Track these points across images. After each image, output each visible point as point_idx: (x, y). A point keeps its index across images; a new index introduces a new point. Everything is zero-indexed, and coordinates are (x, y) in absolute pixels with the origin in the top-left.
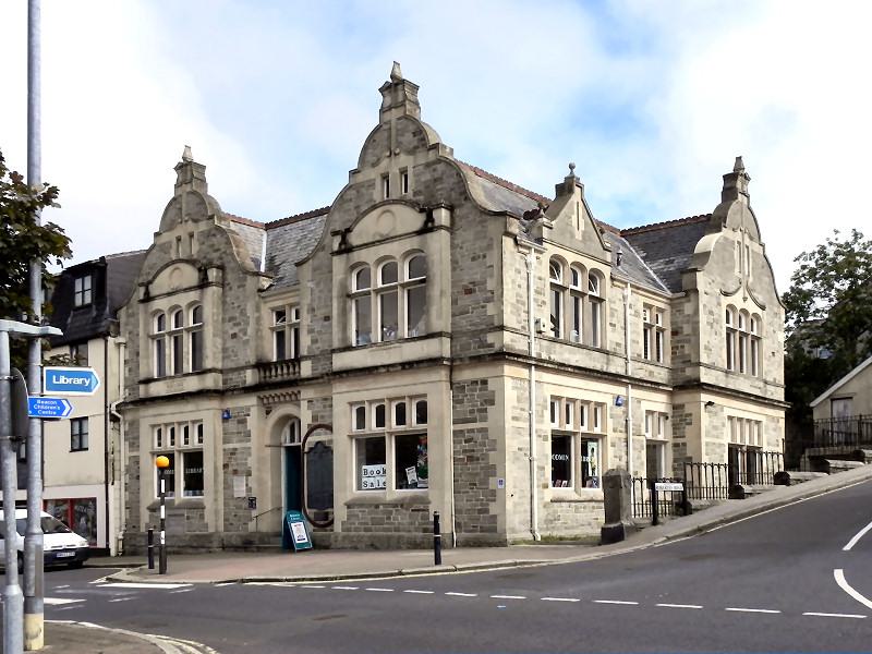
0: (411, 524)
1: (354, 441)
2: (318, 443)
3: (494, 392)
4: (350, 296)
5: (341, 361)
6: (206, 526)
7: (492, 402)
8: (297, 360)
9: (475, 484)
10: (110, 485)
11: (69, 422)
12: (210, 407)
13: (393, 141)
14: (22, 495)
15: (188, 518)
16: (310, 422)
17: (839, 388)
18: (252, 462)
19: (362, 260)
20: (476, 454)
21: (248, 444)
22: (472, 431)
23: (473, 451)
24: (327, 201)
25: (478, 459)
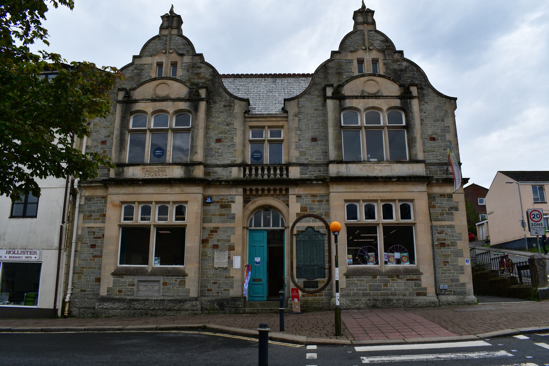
4: (342, 127)
5: (334, 170)
6: (188, 291)
9: (448, 262)
10: (62, 251)
14: (20, 252)
16: (299, 212)
17: (74, 267)
20: (447, 242)
21: (232, 225)
22: (443, 226)
23: (445, 240)
25: (448, 245)
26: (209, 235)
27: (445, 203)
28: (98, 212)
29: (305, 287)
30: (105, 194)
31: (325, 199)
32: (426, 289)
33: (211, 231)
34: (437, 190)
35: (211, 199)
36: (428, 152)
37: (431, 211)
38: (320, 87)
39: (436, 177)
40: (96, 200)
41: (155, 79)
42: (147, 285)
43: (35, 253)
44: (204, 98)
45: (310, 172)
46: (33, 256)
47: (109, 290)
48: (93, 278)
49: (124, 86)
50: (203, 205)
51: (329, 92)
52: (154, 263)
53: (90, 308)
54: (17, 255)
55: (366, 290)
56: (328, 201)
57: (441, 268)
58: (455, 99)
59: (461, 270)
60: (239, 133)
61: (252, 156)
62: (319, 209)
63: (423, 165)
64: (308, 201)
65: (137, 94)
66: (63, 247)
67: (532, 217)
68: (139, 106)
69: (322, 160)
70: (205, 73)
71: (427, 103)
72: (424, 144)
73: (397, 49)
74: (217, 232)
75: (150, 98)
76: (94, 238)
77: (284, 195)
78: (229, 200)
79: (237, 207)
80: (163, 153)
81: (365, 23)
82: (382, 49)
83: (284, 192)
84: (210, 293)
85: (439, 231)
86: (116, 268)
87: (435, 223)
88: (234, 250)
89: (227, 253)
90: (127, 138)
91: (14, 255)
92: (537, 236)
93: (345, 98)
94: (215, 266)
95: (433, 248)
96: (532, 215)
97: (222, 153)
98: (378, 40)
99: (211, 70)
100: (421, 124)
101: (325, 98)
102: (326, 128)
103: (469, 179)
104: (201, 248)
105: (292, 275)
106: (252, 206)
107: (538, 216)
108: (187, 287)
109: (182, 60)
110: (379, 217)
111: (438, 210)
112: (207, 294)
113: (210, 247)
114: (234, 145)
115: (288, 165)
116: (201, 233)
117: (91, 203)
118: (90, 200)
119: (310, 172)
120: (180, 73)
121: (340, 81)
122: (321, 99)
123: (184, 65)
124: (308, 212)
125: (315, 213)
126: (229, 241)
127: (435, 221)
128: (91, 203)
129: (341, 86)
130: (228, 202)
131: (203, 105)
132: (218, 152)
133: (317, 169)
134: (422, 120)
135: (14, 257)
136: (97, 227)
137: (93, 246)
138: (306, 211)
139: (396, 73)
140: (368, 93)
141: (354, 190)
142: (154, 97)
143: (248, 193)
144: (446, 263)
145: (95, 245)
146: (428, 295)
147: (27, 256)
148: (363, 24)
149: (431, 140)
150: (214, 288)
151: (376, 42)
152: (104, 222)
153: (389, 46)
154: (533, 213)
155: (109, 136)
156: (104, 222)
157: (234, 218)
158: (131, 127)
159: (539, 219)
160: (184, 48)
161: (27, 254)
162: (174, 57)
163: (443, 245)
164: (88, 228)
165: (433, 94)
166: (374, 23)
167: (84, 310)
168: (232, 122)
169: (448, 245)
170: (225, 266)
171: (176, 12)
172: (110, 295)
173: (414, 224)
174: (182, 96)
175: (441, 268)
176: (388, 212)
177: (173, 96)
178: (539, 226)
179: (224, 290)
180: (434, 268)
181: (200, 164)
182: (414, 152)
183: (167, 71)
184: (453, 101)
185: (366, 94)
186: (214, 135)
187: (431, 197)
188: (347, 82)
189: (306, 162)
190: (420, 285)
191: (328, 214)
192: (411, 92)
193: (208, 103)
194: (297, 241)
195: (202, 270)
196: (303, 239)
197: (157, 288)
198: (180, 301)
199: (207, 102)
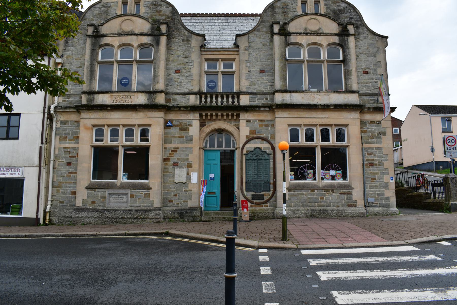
5: (279, 98)
8: (239, 94)
12: (92, 117)
14: (5, 169)
15: (132, 196)
20: (375, 162)
21: (190, 146)
22: (372, 148)
25: (376, 165)
26: (170, 154)
27: (375, 128)
28: (72, 135)
29: (253, 199)
30: (78, 119)
31: (271, 123)
32: (356, 201)
33: (172, 151)
34: (368, 117)
35: (172, 123)
38: (268, 24)
42: (117, 198)
43: (18, 170)
44: (165, 33)
45: (258, 99)
46: (17, 173)
47: (84, 201)
48: (69, 191)
49: (93, 22)
51: (276, 29)
52: (122, 178)
54: (3, 172)
55: (305, 202)
56: (273, 125)
58: (387, 37)
59: (387, 186)
60: (196, 64)
61: (207, 85)
62: (266, 132)
63: (357, 95)
64: (256, 125)
66: (42, 165)
67: (448, 142)
71: (362, 40)
72: (358, 76)
74: (176, 151)
75: (116, 32)
76: (69, 157)
77: (235, 120)
78: (187, 124)
80: (128, 82)
83: (235, 117)
86: (89, 183)
87: (365, 146)
88: (192, 167)
90: (96, 68)
93: (289, 34)
94: (175, 181)
95: (363, 167)
96: (448, 140)
99: (171, 8)
101: (273, 34)
103: (396, 108)
104: (163, 166)
106: (207, 129)
108: (151, 199)
110: (317, 140)
111: (368, 135)
112: (168, 205)
114: (191, 76)
115: (239, 94)
118: (65, 124)
122: (269, 35)
123: (146, 3)
124: (256, 135)
125: (263, 136)
126: (187, 159)
129: (286, 24)
130: (186, 125)
131: (164, 39)
132: (177, 82)
133: (264, 97)
134: (357, 55)
137: (69, 164)
138: (255, 133)
140: (311, 31)
141: (296, 116)
142: (120, 32)
143: (204, 117)
144: (374, 180)
145: (71, 163)
146: (358, 207)
147: (11, 172)
150: (175, 199)
155: (80, 67)
156: (78, 143)
157: (191, 140)
158: (100, 59)
159: (453, 144)
161: (11, 171)
163: (371, 164)
164: (64, 148)
165: (367, 33)
167: (63, 218)
168: (190, 55)
169: (376, 165)
170: (184, 181)
172: (85, 205)
176: (325, 136)
177: (137, 31)
178: (453, 150)
179: (184, 201)
180: (364, 184)
181: (161, 92)
182: (349, 83)
184: (384, 39)
185: (308, 31)
186: (174, 66)
187: (363, 123)
188: (292, 20)
190: (351, 198)
191: (273, 137)
192: (348, 30)
193: (168, 38)
194: (246, 160)
195: (164, 184)
196: (252, 158)
197: (125, 200)
198: (145, 211)
199: (167, 37)
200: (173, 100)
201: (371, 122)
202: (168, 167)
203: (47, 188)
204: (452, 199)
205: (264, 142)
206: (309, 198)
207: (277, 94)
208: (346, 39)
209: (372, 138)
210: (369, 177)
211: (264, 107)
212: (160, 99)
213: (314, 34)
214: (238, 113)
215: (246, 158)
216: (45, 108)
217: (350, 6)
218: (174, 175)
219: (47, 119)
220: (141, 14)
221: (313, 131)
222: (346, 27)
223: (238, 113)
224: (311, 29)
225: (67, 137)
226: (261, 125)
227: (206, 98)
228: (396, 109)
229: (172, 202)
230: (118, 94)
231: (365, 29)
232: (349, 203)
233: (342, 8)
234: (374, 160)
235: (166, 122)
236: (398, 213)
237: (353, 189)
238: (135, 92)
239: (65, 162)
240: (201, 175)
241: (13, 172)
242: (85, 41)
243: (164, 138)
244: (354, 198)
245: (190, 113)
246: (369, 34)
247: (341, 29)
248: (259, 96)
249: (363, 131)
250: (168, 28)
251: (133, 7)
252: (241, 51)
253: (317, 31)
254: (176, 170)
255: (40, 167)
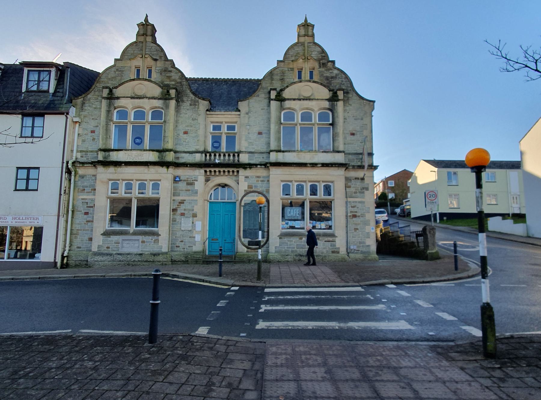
0: (324, 248)
1: (109, 199)
2: (253, 201)
3: (368, 184)
5: (274, 157)
7: (367, 189)
8: (239, 153)
11: (15, 170)
13: (306, 52)
14: (24, 218)
16: (246, 189)
17: (71, 230)
18: (197, 209)
19: (292, 107)
20: (357, 214)
21: (195, 198)
22: (356, 202)
24: (188, 76)
25: (359, 217)
26: (178, 205)
27: (358, 184)
28: (90, 187)
29: (249, 245)
30: (94, 173)
31: (266, 180)
32: (339, 248)
33: (180, 203)
34: (353, 174)
35: (179, 178)
36: (348, 144)
37: (347, 190)
38: (266, 91)
39: (353, 164)
40: (88, 178)
41: (134, 80)
42: (129, 243)
43: (37, 219)
44: (174, 98)
45: (256, 158)
46: (36, 221)
47: (99, 247)
48: (86, 238)
49: (108, 85)
50: (174, 183)
51: (273, 94)
52: (133, 227)
53: (84, 261)
54: (22, 221)
55: (294, 248)
56: (268, 181)
57: (353, 233)
58: (374, 102)
59: (368, 235)
60: (202, 127)
61: (213, 145)
62: (262, 187)
63: (343, 154)
64: (253, 181)
65: (118, 92)
66: (61, 214)
67: (429, 196)
68: (122, 102)
69: (264, 149)
70: (175, 76)
71: (351, 105)
72: (345, 138)
73: (330, 60)
74: (183, 203)
75: (129, 96)
76: (87, 207)
77: (236, 176)
78: (193, 179)
79: (200, 185)
80: (141, 142)
81: (306, 35)
82: (318, 59)
83: (235, 174)
84: (178, 249)
85: (353, 206)
86: (105, 230)
87: (350, 200)
88: (196, 217)
89: (191, 219)
90: (111, 128)
91: (19, 221)
92: (432, 211)
93: (284, 100)
94: (182, 229)
95: (347, 219)
97: (188, 142)
98: (316, 51)
99: (180, 74)
100: (344, 122)
101: (270, 99)
102: (269, 124)
103: (378, 166)
104: (171, 215)
105: (240, 236)
106: (211, 184)
107: (434, 196)
108: (160, 244)
109: (156, 65)
110: (307, 195)
111: (352, 190)
112: (176, 250)
113: (178, 214)
114: (197, 136)
115: (239, 153)
116: (172, 204)
117: (84, 180)
118: (83, 178)
119: (256, 158)
120: (154, 76)
121: (283, 86)
122: (266, 101)
123: (157, 69)
124: (253, 189)
125: (259, 190)
126: (193, 210)
127: (350, 197)
128: (84, 180)
129: (282, 90)
130: (193, 180)
131: (173, 103)
132: (185, 142)
133: (261, 156)
134: (345, 119)
135: (19, 222)
136: (90, 199)
137: (86, 213)
138: (252, 188)
139: (328, 80)
140: (304, 97)
141: (288, 173)
142: (133, 95)
143: (208, 173)
144: (356, 229)
145: (88, 213)
147: (31, 221)
148: (305, 36)
149: (351, 135)
150: (181, 245)
151: (313, 53)
152: (95, 195)
153: (324, 56)
154: (430, 193)
155: (97, 126)
156: (95, 195)
157: (197, 193)
158: (115, 120)
160: (158, 54)
161: (31, 220)
162: (149, 62)
163: (354, 216)
164: (82, 199)
165: (355, 97)
166: (313, 36)
167: (80, 262)
168: (197, 118)
169: (359, 217)
170: (190, 229)
171: (151, 21)
172: (100, 250)
173: (333, 200)
174: (156, 96)
175: (353, 233)
176: (314, 191)
177: (148, 96)
179: (189, 247)
180: (347, 233)
181: (170, 150)
182: (336, 144)
183: (144, 74)
184: (372, 103)
185: (302, 97)
186: (182, 127)
187: (347, 179)
188: (287, 87)
189: (253, 151)
190: (335, 245)
191: (268, 191)
192: (337, 96)
193: (177, 101)
194: (244, 211)
195: (172, 232)
196: (249, 210)
197: (137, 245)
198: (155, 255)
199: (176, 101)
200: (181, 158)
201: (356, 178)
202: (175, 217)
203: (66, 234)
204: (430, 248)
205: (260, 195)
206: (297, 245)
207: (271, 153)
208: (335, 104)
209: (355, 193)
210: (351, 227)
211: (261, 165)
212: (170, 157)
213: (307, 99)
214: (238, 170)
215: (244, 209)
216: (63, 163)
217: (342, 73)
218: (181, 224)
219: (66, 173)
220: (152, 79)
221: (302, 186)
222: (336, 93)
223: (238, 170)
224: (305, 96)
225: (85, 189)
226: (258, 181)
227: (210, 155)
228: (379, 167)
229: (179, 247)
230: (131, 152)
231: (354, 94)
232: (333, 250)
233: (334, 75)
234: (356, 212)
235: (175, 178)
236: (377, 259)
237: (337, 237)
238: (147, 150)
239: (83, 212)
240: (205, 224)
241: (32, 221)
242: (101, 102)
243: (172, 191)
244: (337, 246)
245: (364, 328)
246: (358, 98)
247: (331, 95)
248: (256, 155)
249: (347, 187)
250: (178, 93)
251: (145, 70)
252: (242, 115)
253: (310, 97)
254: (183, 219)
255: (59, 216)
